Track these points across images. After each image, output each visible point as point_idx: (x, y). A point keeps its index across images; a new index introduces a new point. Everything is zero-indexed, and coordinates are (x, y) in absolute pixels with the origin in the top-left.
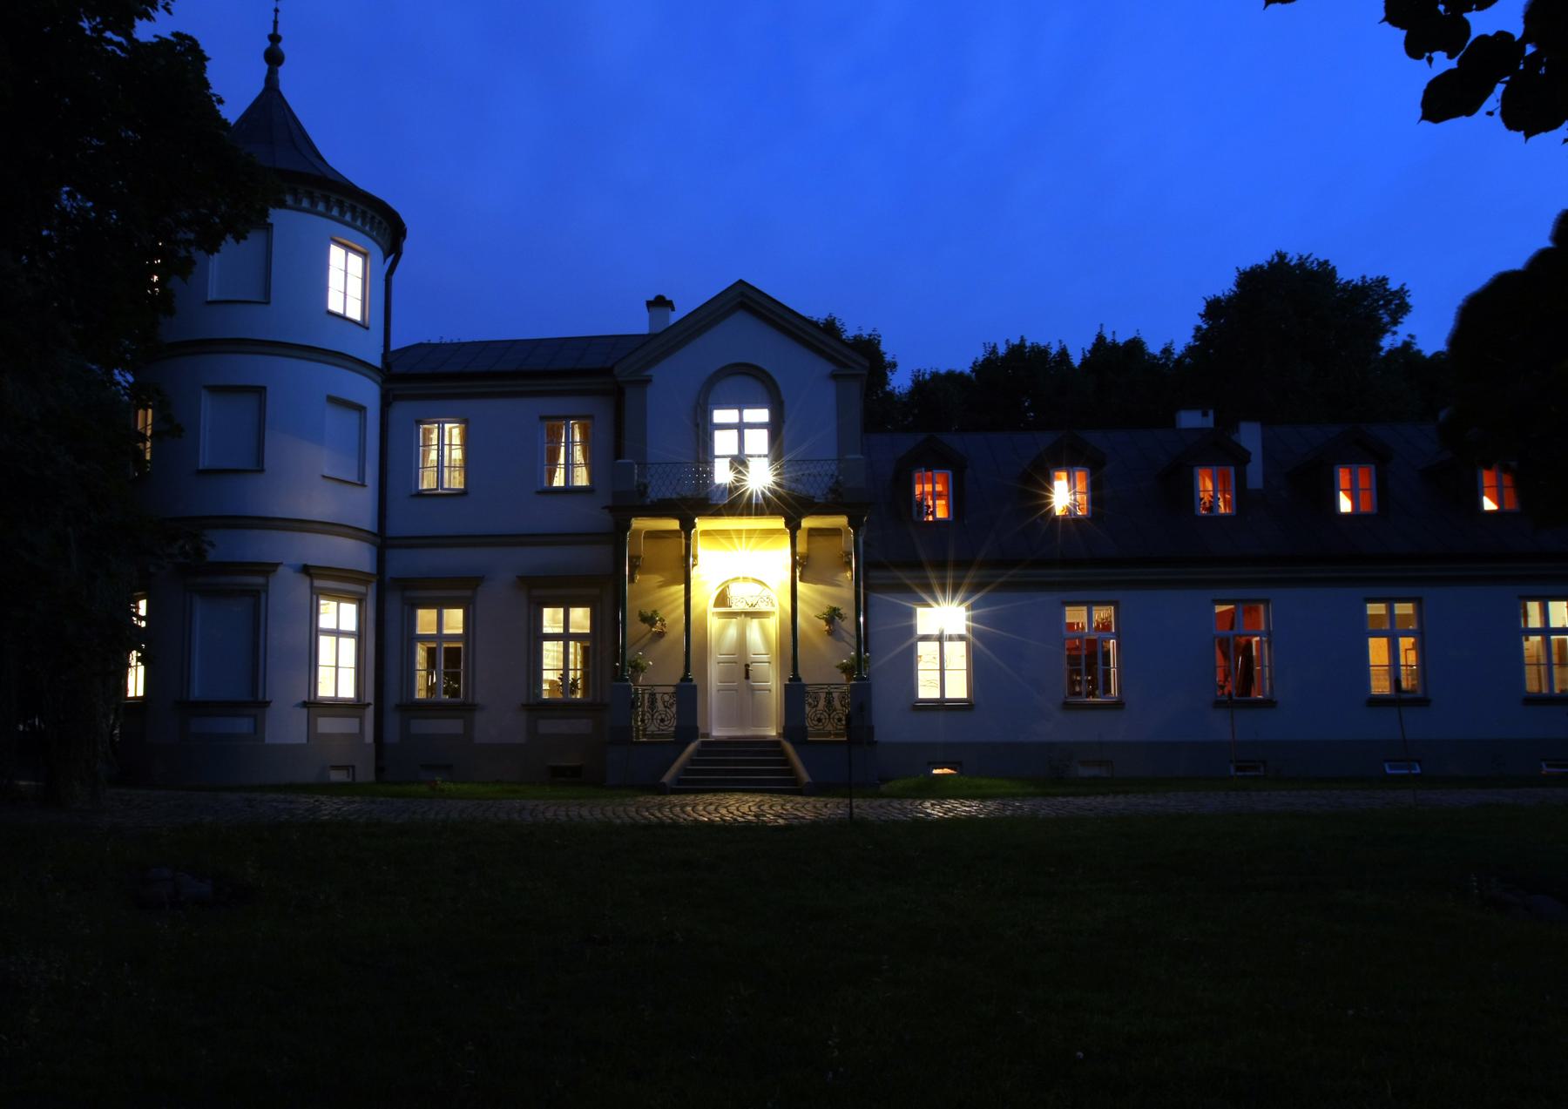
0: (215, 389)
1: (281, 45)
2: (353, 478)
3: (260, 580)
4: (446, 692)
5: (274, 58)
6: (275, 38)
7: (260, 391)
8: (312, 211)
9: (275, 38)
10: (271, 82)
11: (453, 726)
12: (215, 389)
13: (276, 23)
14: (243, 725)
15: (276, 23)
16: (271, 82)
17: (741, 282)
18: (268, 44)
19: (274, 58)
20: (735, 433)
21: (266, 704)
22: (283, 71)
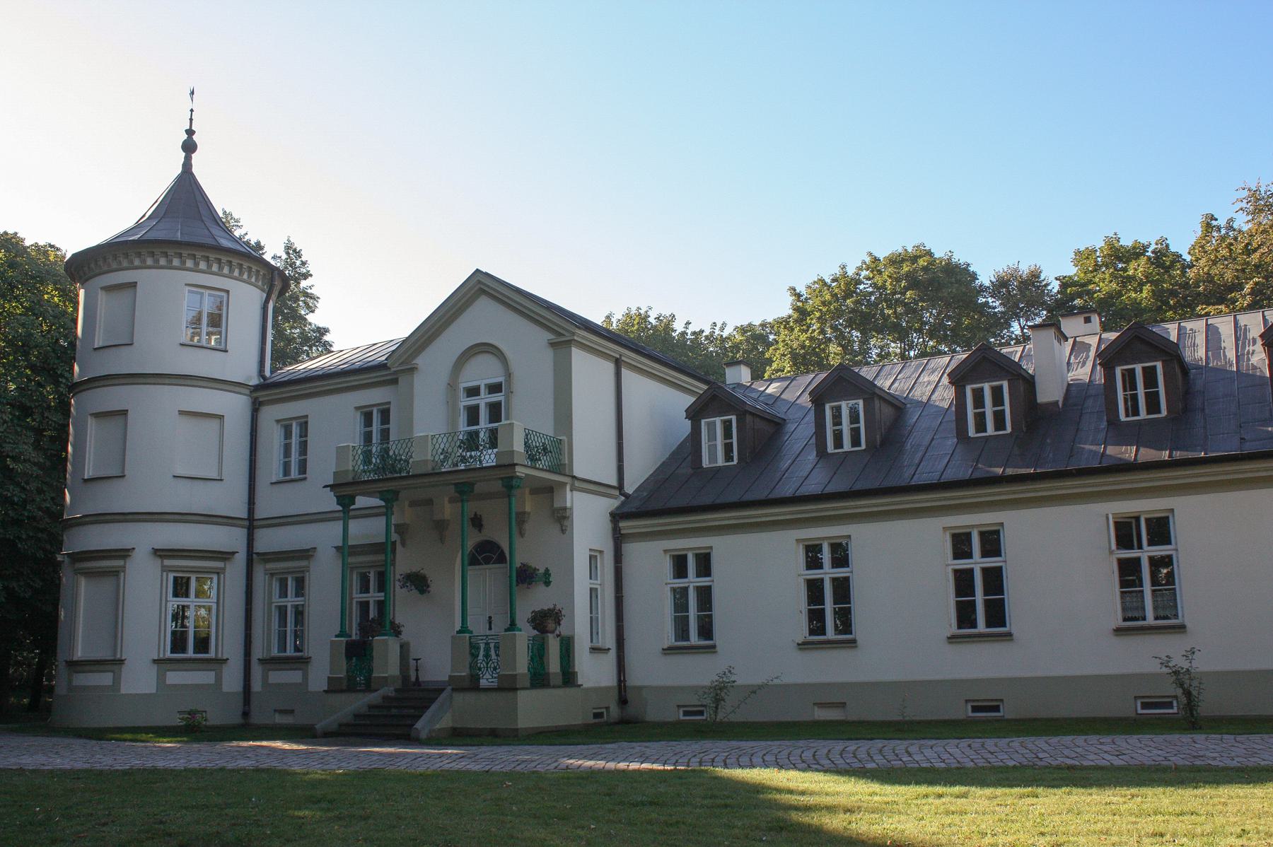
0: (97, 415)
1: (195, 137)
2: (215, 475)
3: (121, 563)
4: (1141, 291)
5: (189, 147)
6: (190, 132)
7: (124, 413)
8: (157, 266)
9: (190, 132)
10: (187, 165)
11: (293, 677)
12: (97, 415)
13: (191, 120)
14: (105, 679)
15: (191, 120)
16: (187, 165)
17: (481, 288)
18: (186, 137)
19: (189, 147)
20: (243, 513)
21: (121, 662)
22: (195, 157)
